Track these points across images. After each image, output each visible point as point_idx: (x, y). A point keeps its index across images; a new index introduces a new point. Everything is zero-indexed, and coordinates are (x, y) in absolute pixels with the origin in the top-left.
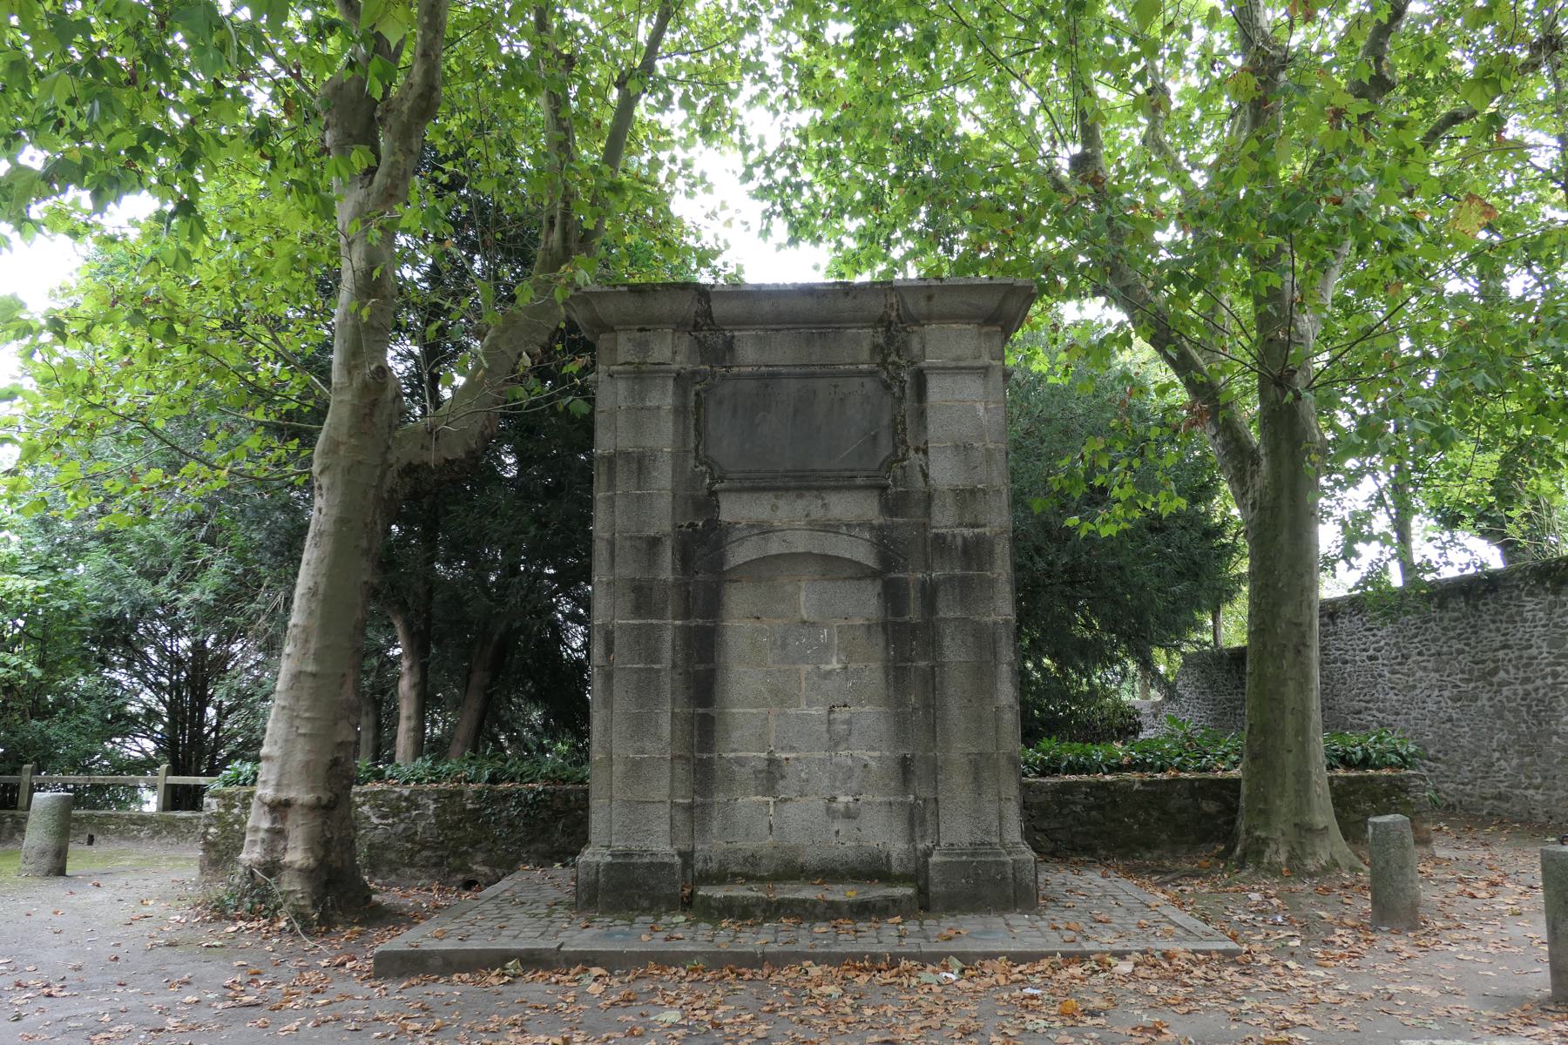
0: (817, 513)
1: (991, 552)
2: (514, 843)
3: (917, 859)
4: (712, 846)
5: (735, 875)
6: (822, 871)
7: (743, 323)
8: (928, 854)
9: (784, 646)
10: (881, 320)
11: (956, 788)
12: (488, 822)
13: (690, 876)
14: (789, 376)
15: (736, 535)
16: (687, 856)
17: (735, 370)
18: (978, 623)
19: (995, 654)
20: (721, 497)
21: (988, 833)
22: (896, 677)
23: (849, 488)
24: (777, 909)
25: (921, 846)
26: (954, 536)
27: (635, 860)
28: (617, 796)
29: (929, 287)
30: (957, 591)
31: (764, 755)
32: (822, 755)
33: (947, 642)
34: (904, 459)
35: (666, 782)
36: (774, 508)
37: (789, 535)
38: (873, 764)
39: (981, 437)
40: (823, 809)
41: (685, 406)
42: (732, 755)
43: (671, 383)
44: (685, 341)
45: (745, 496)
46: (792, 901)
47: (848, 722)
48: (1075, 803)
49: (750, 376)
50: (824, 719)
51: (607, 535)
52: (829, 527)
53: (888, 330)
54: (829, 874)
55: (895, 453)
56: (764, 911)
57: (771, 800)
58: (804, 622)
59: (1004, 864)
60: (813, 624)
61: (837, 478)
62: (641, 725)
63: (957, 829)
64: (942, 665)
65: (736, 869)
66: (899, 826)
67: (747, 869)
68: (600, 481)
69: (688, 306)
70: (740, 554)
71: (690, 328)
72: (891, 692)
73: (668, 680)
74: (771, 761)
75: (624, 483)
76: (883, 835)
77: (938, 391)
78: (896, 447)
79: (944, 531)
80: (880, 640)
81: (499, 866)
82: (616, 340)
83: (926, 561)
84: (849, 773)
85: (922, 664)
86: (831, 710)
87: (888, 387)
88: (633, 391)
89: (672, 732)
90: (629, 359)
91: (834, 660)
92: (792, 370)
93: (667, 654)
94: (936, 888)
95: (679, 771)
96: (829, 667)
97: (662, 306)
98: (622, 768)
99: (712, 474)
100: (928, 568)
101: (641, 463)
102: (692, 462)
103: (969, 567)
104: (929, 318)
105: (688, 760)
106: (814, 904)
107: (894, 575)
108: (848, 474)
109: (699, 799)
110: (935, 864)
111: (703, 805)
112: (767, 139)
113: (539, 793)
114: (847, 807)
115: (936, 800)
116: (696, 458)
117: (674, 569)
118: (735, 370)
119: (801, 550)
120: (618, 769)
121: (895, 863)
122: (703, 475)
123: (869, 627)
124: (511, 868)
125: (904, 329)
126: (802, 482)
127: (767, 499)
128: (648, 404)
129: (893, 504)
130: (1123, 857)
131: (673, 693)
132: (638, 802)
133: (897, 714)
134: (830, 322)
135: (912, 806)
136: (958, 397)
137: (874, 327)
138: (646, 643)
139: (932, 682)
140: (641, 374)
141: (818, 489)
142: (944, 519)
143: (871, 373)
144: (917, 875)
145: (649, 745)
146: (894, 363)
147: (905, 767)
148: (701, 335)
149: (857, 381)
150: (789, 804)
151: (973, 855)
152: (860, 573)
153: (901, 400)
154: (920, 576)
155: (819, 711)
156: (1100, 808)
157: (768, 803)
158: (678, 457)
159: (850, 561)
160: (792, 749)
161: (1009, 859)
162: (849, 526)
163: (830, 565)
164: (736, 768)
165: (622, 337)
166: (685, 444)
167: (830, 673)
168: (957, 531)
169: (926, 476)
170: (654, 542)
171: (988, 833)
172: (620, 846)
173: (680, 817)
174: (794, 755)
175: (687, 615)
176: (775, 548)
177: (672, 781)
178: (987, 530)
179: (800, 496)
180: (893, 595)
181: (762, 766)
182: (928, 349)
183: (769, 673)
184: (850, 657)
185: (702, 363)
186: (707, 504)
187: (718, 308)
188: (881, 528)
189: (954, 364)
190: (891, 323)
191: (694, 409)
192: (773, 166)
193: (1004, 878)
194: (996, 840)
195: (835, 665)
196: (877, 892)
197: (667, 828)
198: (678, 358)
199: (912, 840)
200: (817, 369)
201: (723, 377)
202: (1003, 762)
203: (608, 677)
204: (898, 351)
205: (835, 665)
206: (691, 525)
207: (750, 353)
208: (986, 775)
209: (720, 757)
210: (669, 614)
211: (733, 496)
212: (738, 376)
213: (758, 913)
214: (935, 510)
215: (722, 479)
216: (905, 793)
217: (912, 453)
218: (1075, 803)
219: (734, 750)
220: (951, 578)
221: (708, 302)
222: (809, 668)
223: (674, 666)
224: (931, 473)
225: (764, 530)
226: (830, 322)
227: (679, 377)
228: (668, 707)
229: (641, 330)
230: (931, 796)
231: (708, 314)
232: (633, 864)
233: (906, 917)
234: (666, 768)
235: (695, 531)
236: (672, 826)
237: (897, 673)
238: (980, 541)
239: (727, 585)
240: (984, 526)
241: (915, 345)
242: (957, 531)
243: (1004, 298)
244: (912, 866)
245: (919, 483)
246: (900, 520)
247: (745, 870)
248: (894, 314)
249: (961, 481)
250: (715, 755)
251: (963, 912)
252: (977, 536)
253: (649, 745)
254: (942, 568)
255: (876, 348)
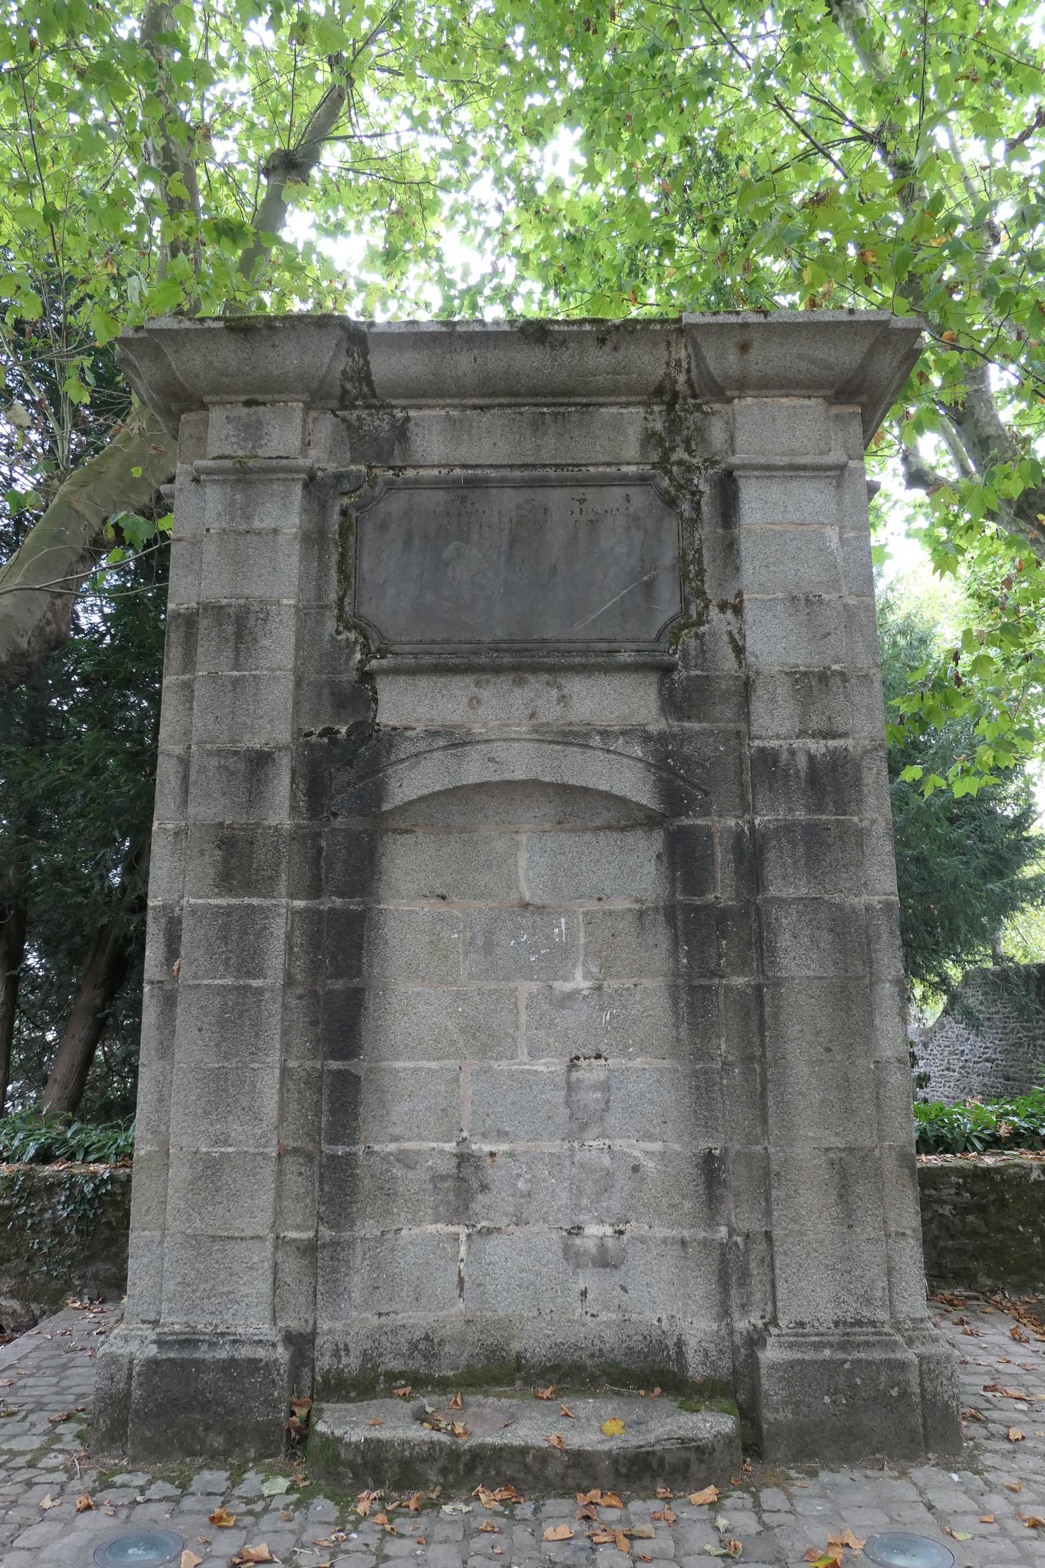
0: (550, 712)
1: (857, 782)
2: (60, 1263)
3: (735, 1350)
4: (348, 1327)
5: (392, 1376)
6: (555, 1368)
7: (424, 395)
8: (755, 1340)
9: (489, 947)
10: (659, 391)
11: (807, 1212)
12: (23, 1228)
13: (307, 1382)
14: (502, 483)
15: (405, 749)
16: (301, 1344)
17: (410, 473)
18: (840, 907)
19: (870, 963)
20: (381, 683)
21: (869, 1302)
22: (691, 1006)
23: (607, 669)
24: (470, 1468)
25: (741, 1325)
26: (792, 753)
27: (203, 1353)
28: (176, 1226)
29: (745, 326)
30: (801, 850)
31: (450, 1147)
32: (555, 1146)
33: (784, 941)
34: (700, 623)
35: (266, 1198)
36: (474, 702)
37: (499, 750)
38: (650, 1166)
39: (834, 585)
40: (558, 1248)
41: (322, 532)
42: (392, 1147)
43: (298, 490)
44: (325, 427)
45: (423, 682)
46: (499, 1453)
47: (605, 1087)
48: (940, 1202)
49: (436, 484)
50: (560, 1080)
51: (178, 750)
52: (572, 737)
53: (671, 406)
54: (570, 1375)
55: (685, 611)
56: (444, 1471)
57: (463, 1231)
58: (526, 906)
59: (902, 1366)
60: (541, 909)
61: (585, 653)
62: (223, 1091)
63: (810, 1294)
64: (777, 983)
65: (395, 1365)
66: (701, 1286)
67: (417, 1364)
68: (173, 654)
69: (326, 360)
70: (409, 783)
71: (334, 403)
72: (683, 1034)
73: (276, 1008)
74: (463, 1159)
75: (212, 657)
76: (670, 1303)
77: (755, 503)
78: (685, 602)
79: (774, 743)
80: (660, 935)
81: (36, 1300)
82: (206, 422)
83: (743, 797)
84: (606, 1183)
85: (739, 981)
86: (573, 1063)
87: (671, 503)
88: (232, 504)
89: (282, 1105)
90: (227, 450)
91: (579, 974)
92: (507, 473)
93: (275, 960)
94: (775, 1414)
95: (295, 1182)
96: (568, 987)
97: (287, 359)
98: (185, 1172)
99: (365, 646)
100: (747, 808)
101: (240, 625)
102: (331, 625)
103: (820, 808)
104: (743, 385)
105: (310, 1157)
106: (544, 1456)
107: (685, 821)
108: (604, 646)
109: (327, 1233)
110: (774, 1366)
111: (334, 1243)
112: (472, 268)
113: (104, 1182)
114: (602, 1247)
115: (768, 1236)
116: (339, 618)
117: (294, 808)
118: (410, 473)
119: (520, 775)
120: (179, 1174)
121: (693, 1359)
122: (350, 646)
123: (641, 914)
124: (55, 1304)
125: (698, 408)
126: (523, 659)
127: (461, 687)
128: (257, 524)
129: (681, 700)
130: (1019, 1289)
131: (285, 1032)
132: (214, 1238)
133: (695, 1074)
134: (571, 393)
135: (725, 1250)
136: (796, 517)
137: (648, 405)
138: (239, 939)
139: (758, 1012)
140: (244, 476)
141: (553, 670)
142: (774, 723)
143: (642, 480)
144: (736, 1386)
145: (236, 1130)
146: (680, 463)
147: (711, 1170)
148: (352, 416)
149: (618, 492)
150: (495, 1240)
151: (843, 1346)
152: (627, 817)
153: (694, 522)
154: (732, 823)
155: (550, 1066)
156: (981, 1209)
157: (456, 1238)
158: (308, 615)
159: (607, 796)
160: (502, 1135)
161: (910, 1355)
162: (605, 734)
163: (571, 802)
164: (398, 1171)
165: (217, 415)
166: (320, 594)
167: (571, 996)
168: (797, 744)
169: (739, 651)
170: (259, 762)
171: (869, 1302)
172: (175, 1324)
173: (292, 1265)
174: (502, 1147)
175: (315, 890)
176: (474, 770)
177: (279, 1197)
178: (849, 743)
179: (520, 683)
180: (685, 857)
181: (447, 1167)
182: (740, 439)
183: (461, 996)
184: (606, 968)
185: (353, 461)
186: (360, 695)
187: (382, 366)
188: (662, 738)
189: (786, 460)
190: (675, 395)
191: (338, 533)
192: (481, 301)
193: (904, 1394)
194: (882, 1315)
195: (579, 982)
196: (669, 1425)
197: (265, 1288)
198: (313, 453)
199: (725, 1313)
200: (551, 473)
201: (390, 486)
202: (890, 1164)
203: (169, 1001)
204: (687, 442)
205: (579, 982)
206: (328, 732)
207: (436, 443)
208: (859, 1189)
209: (369, 1152)
210: (282, 887)
211: (402, 681)
212: (415, 484)
213: (433, 1476)
214: (758, 707)
215: (383, 653)
216: (711, 1219)
217: (714, 612)
218: (940, 1202)
219: (395, 1139)
220: (788, 828)
221: (364, 354)
222: (534, 987)
223: (290, 981)
224: (749, 644)
225: (456, 740)
226: (571, 393)
227: (311, 482)
228: (274, 1058)
229: (248, 404)
230: (757, 1227)
231: (365, 376)
232: (197, 1363)
233: (724, 1481)
234: (267, 1173)
235: (334, 742)
236: (276, 1283)
237: (693, 998)
238: (838, 761)
239: (389, 839)
240: (844, 735)
241: (717, 434)
242: (797, 744)
243: (870, 355)
244: (726, 1363)
245: (728, 662)
246: (696, 726)
247: (412, 1365)
248: (682, 378)
249: (802, 659)
250: (360, 1149)
251: (831, 1464)
252: (834, 753)
253: (236, 1130)
254: (773, 809)
255: (649, 438)
